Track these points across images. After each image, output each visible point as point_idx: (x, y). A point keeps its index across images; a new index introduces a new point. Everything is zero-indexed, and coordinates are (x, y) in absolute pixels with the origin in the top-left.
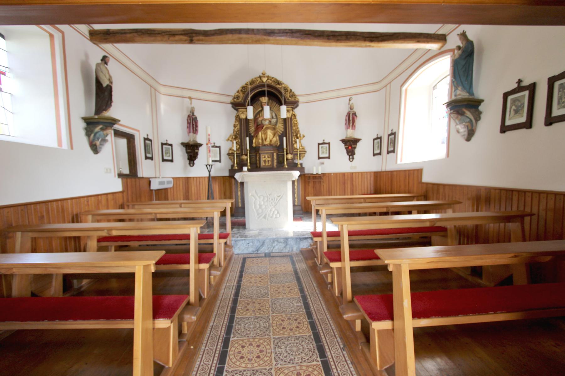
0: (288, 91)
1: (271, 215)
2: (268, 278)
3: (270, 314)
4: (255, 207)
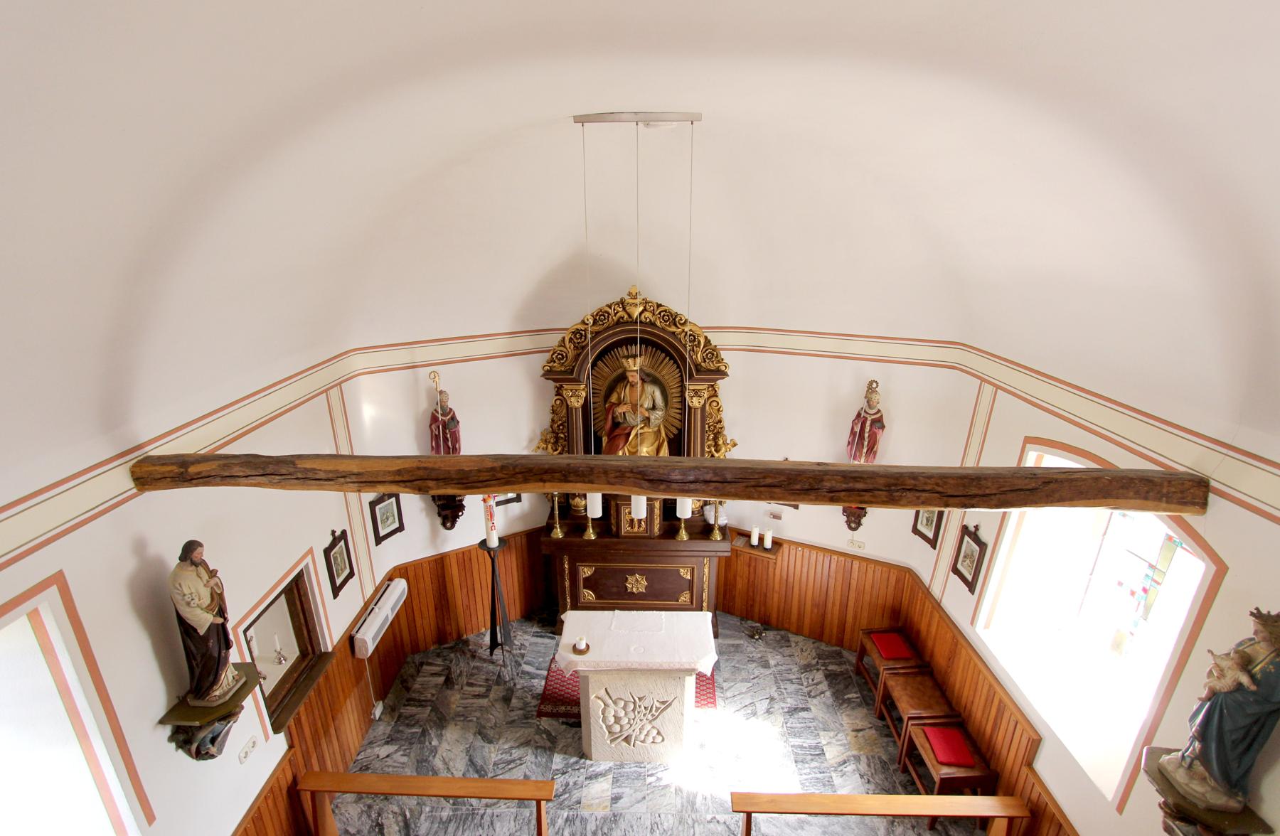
1: (642, 737)
4: (604, 720)
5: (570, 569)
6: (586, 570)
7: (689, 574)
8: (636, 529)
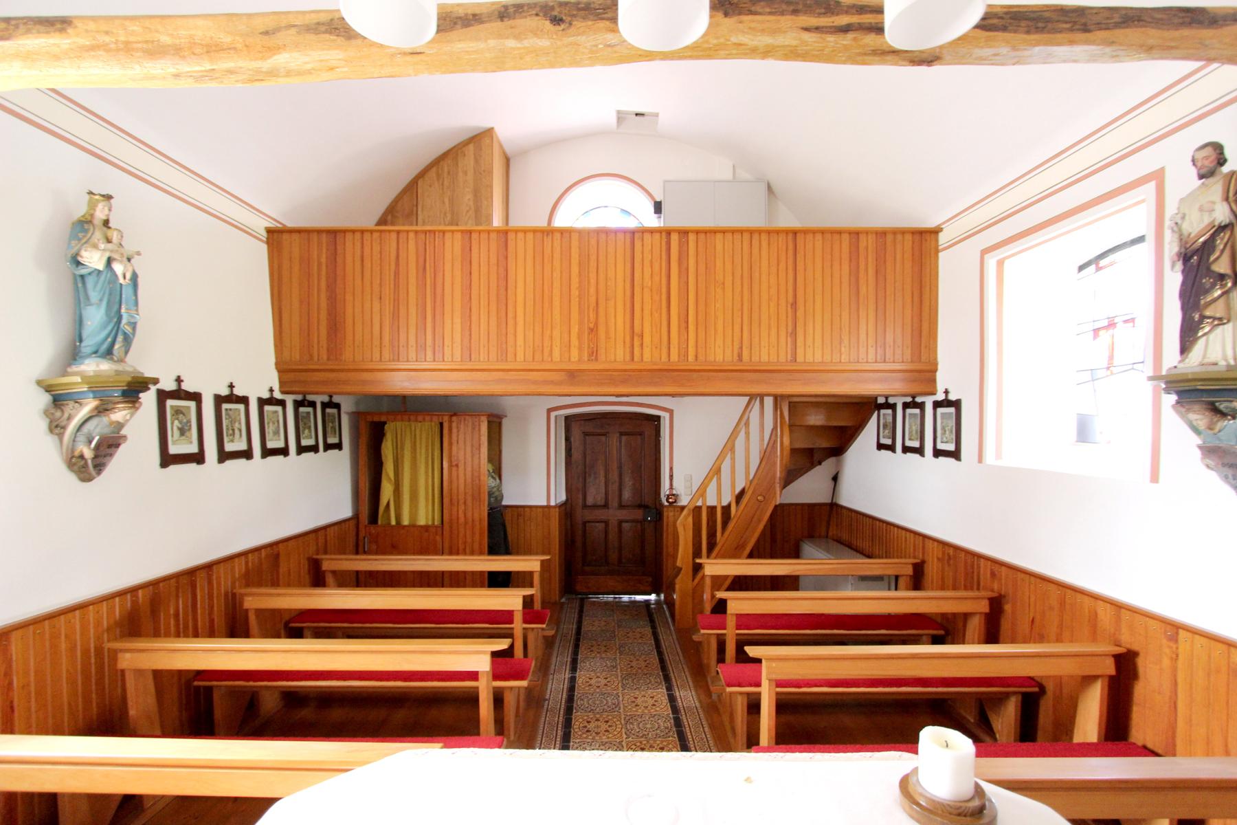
2: (621, 723)
3: (624, 738)
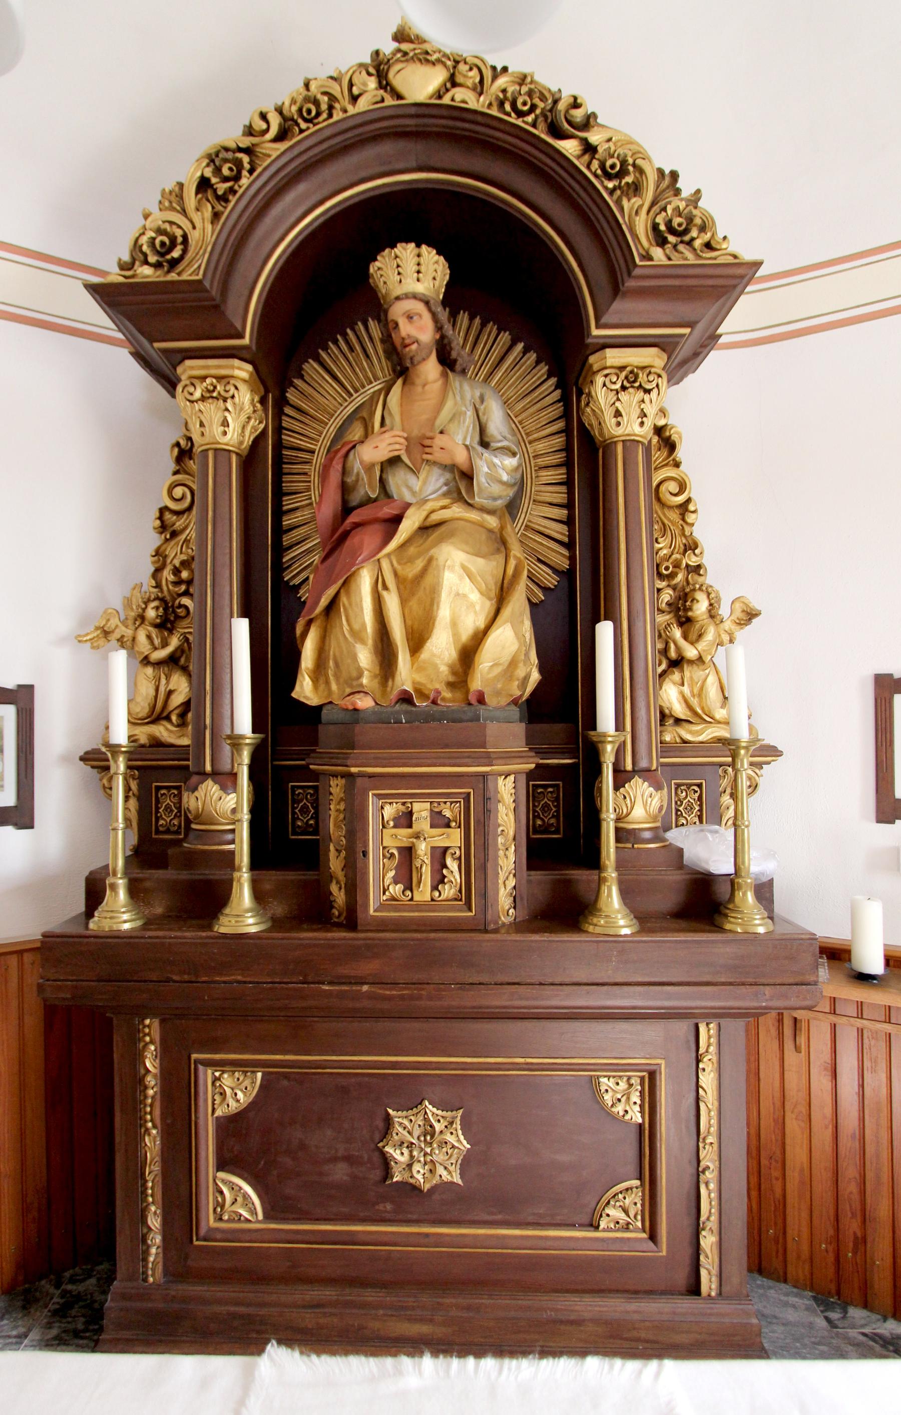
0: (636, 189)
5: (167, 1076)
6: (227, 1080)
7: (635, 1097)
8: (424, 893)
